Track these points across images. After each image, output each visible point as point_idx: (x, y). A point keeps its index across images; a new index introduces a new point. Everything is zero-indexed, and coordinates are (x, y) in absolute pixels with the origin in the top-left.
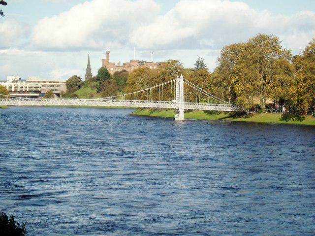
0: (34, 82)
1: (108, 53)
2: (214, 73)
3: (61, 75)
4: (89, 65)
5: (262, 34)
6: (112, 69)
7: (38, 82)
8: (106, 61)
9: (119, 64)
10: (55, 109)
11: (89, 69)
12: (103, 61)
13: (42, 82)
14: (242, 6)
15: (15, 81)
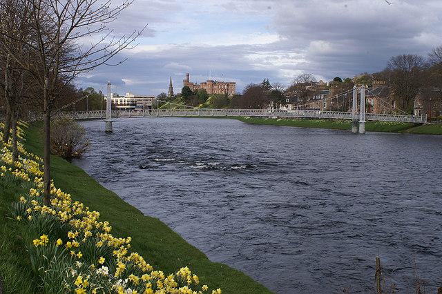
15: (114, 97)
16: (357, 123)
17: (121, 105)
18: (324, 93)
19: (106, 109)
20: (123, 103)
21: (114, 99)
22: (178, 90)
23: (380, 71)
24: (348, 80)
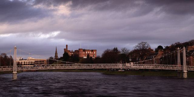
0: (31, 60)
3: (46, 58)
4: (56, 52)
5: (177, 42)
7: (33, 60)
9: (72, 51)
11: (56, 53)
13: (34, 60)
14: (88, 16)
15: (21, 60)
16: (182, 72)
17: (24, 65)
20: (26, 63)
21: (20, 61)
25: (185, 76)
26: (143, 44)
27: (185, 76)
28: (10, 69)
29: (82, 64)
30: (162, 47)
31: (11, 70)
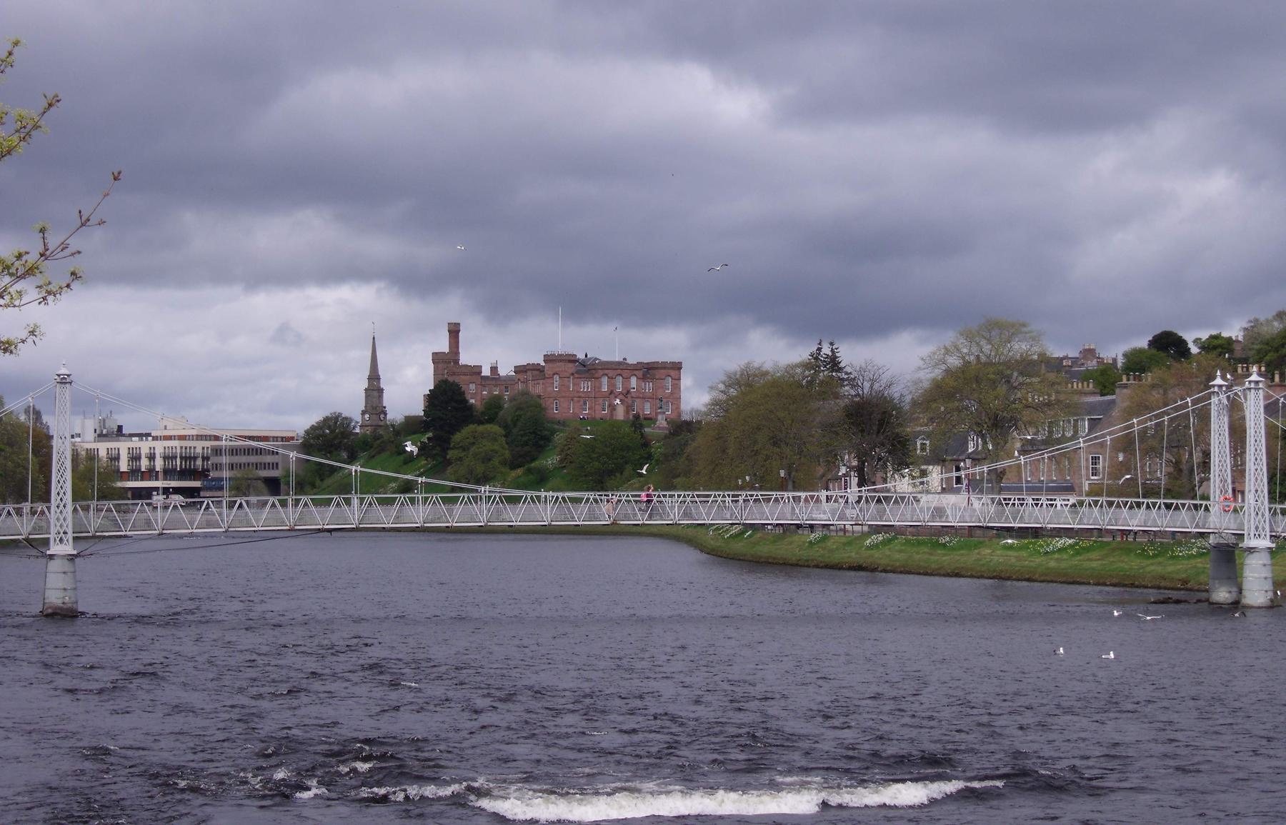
1: (454, 332)
2: (483, 413)
4: (374, 377)
6: (472, 386)
8: (446, 362)
10: (144, 543)
11: (374, 390)
12: (438, 358)
15: (101, 436)
16: (1228, 556)
17: (135, 473)
18: (1092, 409)
19: (48, 500)
20: (144, 464)
21: (103, 448)
22: (408, 391)
23: (768, 366)
24: (1267, 320)
25: (1257, 583)
26: (1001, 329)
27: (1257, 583)
28: (22, 527)
29: (529, 494)
30: (1184, 343)
31: (36, 530)
